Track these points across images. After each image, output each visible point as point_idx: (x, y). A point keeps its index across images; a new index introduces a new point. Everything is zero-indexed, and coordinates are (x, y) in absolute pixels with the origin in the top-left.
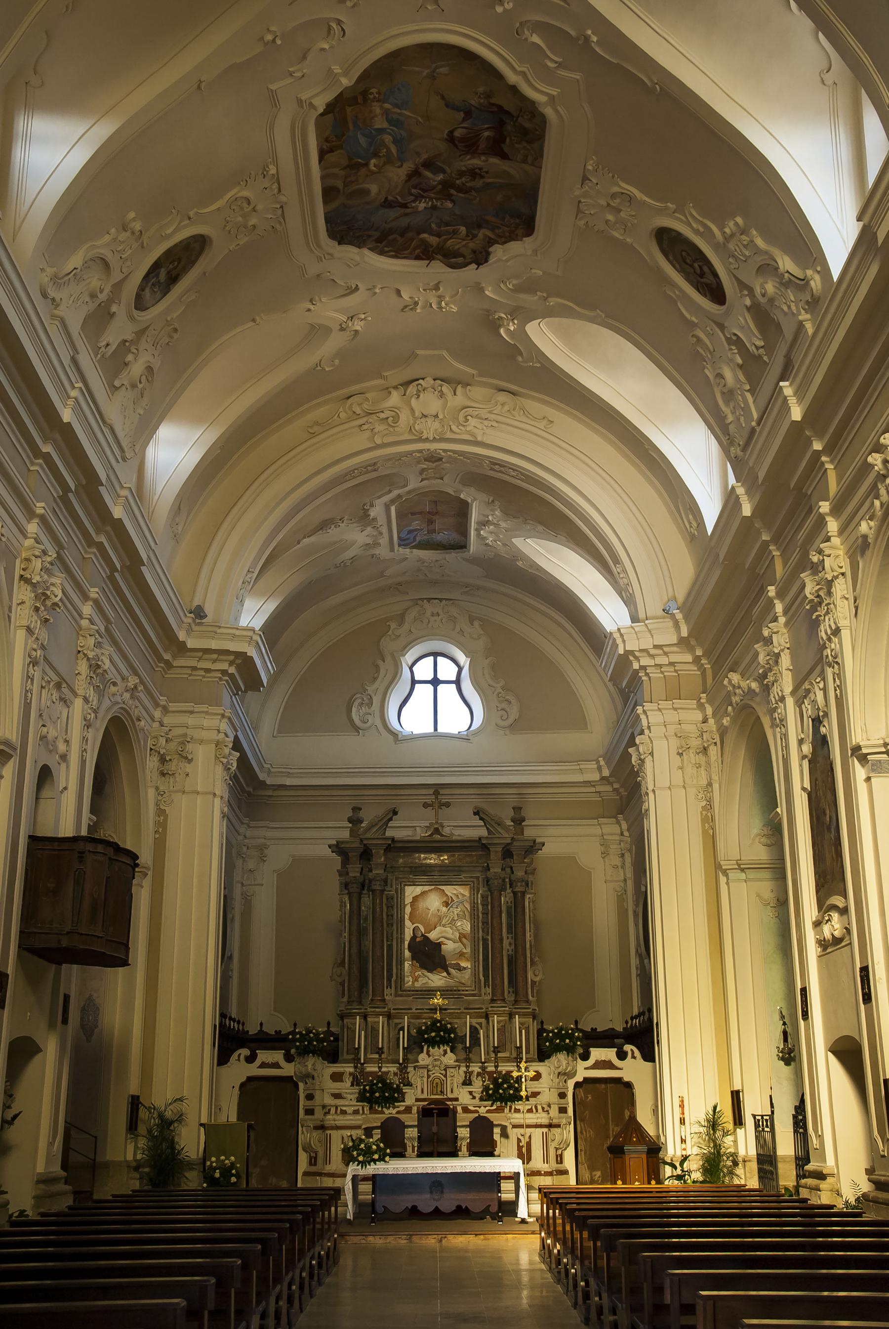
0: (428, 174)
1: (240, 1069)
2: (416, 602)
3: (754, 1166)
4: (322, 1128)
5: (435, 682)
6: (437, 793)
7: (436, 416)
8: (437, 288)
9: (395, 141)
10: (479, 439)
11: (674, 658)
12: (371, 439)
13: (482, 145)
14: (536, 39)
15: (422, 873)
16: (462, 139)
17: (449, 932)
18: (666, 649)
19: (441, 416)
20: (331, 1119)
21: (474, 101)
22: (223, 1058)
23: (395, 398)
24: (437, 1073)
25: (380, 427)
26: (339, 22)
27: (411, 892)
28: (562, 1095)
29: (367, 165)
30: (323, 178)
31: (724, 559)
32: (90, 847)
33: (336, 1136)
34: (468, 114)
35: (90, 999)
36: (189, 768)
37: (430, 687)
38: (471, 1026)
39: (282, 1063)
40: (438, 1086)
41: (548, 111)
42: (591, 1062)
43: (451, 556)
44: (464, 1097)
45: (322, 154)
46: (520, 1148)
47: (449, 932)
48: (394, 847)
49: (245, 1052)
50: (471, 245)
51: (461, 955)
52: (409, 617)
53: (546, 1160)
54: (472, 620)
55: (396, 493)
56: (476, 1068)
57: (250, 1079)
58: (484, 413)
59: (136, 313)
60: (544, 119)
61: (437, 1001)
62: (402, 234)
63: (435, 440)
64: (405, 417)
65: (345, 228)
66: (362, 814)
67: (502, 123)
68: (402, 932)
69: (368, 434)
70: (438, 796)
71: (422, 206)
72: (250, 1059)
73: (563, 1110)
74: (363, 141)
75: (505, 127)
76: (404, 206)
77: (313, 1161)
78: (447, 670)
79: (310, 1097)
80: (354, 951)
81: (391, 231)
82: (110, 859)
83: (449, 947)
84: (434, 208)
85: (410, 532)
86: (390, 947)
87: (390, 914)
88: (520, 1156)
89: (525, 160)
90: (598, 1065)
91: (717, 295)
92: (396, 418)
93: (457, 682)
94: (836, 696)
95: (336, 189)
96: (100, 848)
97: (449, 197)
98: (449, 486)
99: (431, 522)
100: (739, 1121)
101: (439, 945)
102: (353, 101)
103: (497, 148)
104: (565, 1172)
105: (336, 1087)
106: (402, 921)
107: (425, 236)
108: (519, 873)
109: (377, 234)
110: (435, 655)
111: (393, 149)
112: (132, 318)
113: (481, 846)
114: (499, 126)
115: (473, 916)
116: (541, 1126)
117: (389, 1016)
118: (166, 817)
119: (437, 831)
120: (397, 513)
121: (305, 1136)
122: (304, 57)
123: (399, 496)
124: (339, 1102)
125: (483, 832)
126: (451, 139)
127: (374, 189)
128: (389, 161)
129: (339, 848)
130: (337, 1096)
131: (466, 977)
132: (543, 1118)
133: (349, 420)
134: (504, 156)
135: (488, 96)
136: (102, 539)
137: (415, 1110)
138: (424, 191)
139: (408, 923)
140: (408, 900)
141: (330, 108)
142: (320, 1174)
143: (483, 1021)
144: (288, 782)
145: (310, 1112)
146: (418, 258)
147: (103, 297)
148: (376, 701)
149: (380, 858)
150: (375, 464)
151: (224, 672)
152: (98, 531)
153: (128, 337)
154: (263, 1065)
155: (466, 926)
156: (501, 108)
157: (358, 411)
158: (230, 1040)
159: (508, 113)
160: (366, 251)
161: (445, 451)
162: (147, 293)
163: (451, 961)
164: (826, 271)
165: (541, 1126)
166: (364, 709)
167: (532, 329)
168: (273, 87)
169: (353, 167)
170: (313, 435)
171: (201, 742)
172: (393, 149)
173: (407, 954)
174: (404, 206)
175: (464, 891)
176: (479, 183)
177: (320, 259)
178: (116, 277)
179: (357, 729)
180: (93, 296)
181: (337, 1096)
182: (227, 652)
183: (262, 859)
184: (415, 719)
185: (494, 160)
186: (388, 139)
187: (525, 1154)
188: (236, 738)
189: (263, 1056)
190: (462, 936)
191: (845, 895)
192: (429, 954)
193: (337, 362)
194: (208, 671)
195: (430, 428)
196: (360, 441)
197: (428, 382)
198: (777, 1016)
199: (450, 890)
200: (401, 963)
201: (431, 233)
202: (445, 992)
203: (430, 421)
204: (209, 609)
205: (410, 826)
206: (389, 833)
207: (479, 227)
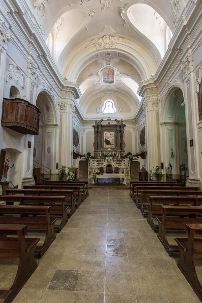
3: (165, 175)
4: (91, 168)
5: (109, 106)
7: (109, 43)
10: (116, 48)
11: (152, 86)
15: (106, 130)
17: (111, 139)
18: (151, 84)
19: (109, 43)
23: (101, 40)
27: (105, 133)
31: (172, 49)
33: (93, 170)
35: (49, 147)
36: (65, 108)
37: (108, 107)
38: (114, 153)
40: (109, 162)
43: (111, 84)
44: (113, 164)
47: (111, 139)
48: (102, 126)
49: (80, 157)
51: (113, 142)
52: (105, 96)
54: (114, 96)
55: (102, 68)
56: (115, 159)
61: (109, 149)
64: (103, 43)
68: (104, 139)
69: (96, 48)
72: (80, 158)
73: (129, 166)
77: (90, 173)
78: (111, 104)
80: (96, 142)
82: (26, 105)
83: (111, 141)
85: (105, 79)
86: (102, 141)
87: (102, 135)
92: (101, 43)
93: (112, 106)
94: (187, 88)
96: (23, 102)
99: (108, 76)
100: (162, 168)
101: (109, 141)
104: (129, 175)
105: (93, 162)
106: (103, 137)
108: (122, 130)
110: (109, 102)
113: (116, 125)
115: (115, 137)
116: (125, 168)
117: (102, 152)
118: (62, 117)
119: (109, 123)
120: (103, 73)
121: (89, 169)
124: (94, 164)
130: (93, 163)
131: (114, 146)
132: (126, 167)
137: (105, 166)
143: (116, 152)
144: (88, 120)
145: (89, 166)
148: (100, 108)
149: (100, 127)
150: (98, 55)
151: (71, 92)
152: (60, 87)
154: (82, 159)
155: (114, 138)
157: (94, 43)
158: (75, 155)
161: (110, 51)
163: (111, 143)
165: (125, 168)
166: (99, 110)
171: (68, 104)
173: (104, 142)
175: (113, 133)
179: (97, 113)
181: (93, 163)
182: (71, 87)
183: (84, 131)
184: (106, 111)
189: (82, 158)
192: (108, 142)
193: (89, 28)
194: (68, 91)
196: (94, 49)
197: (107, 36)
199: (111, 132)
200: (103, 144)
202: (110, 148)
203: (107, 44)
206: (101, 123)
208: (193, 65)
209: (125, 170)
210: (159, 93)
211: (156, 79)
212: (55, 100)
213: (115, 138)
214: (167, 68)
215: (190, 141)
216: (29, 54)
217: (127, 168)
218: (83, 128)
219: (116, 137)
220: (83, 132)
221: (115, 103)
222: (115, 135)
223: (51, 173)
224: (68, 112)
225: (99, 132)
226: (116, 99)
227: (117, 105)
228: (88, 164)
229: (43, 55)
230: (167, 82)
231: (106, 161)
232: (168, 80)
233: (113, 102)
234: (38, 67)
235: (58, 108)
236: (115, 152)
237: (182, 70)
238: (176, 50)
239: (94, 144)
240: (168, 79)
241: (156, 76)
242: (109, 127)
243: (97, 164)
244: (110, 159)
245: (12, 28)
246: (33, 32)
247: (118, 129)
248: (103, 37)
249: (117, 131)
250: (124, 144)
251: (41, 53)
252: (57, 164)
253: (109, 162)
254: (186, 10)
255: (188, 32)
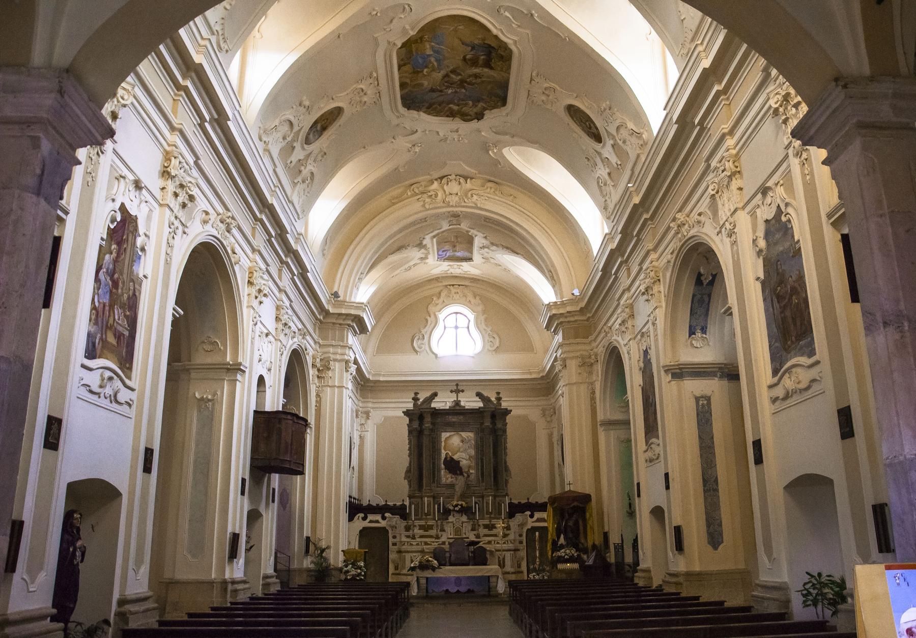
0: (453, 76)
1: (359, 523)
2: (446, 286)
4: (399, 552)
5: (456, 327)
6: (457, 385)
8: (457, 131)
9: (436, 61)
12: (424, 206)
13: (481, 62)
14: (507, 14)
16: (470, 60)
20: (404, 548)
21: (476, 42)
22: (351, 519)
23: (436, 185)
24: (457, 525)
25: (428, 200)
26: (409, 5)
27: (444, 435)
28: (521, 535)
29: (422, 71)
30: (400, 78)
32: (284, 416)
33: (408, 557)
34: (473, 48)
39: (380, 520)
41: (513, 48)
42: (535, 518)
45: (400, 67)
46: (499, 561)
47: (464, 455)
48: (436, 413)
49: (362, 515)
50: (475, 110)
51: (470, 467)
52: (443, 294)
53: (512, 566)
57: (364, 528)
58: (481, 193)
59: (306, 146)
60: (511, 51)
62: (440, 105)
63: (456, 206)
64: (440, 194)
65: (411, 101)
66: (419, 396)
67: (490, 53)
68: (440, 453)
70: (457, 387)
71: (450, 91)
72: (364, 519)
74: (420, 61)
75: (492, 54)
76: (441, 91)
77: (396, 568)
79: (394, 537)
81: (434, 104)
83: (464, 463)
84: (456, 92)
88: (500, 565)
89: (502, 70)
90: (539, 520)
91: (598, 138)
92: (436, 195)
93: (468, 328)
95: (406, 83)
97: (464, 87)
98: (464, 226)
101: (459, 462)
102: (416, 42)
103: (488, 64)
104: (522, 572)
107: (451, 106)
108: (499, 425)
109: (427, 105)
111: (435, 64)
112: (303, 149)
114: (489, 54)
116: (509, 550)
121: (393, 556)
122: (391, 21)
123: (438, 234)
125: (481, 405)
126: (464, 59)
127: (426, 83)
128: (434, 70)
129: (407, 413)
132: (511, 546)
133: (412, 196)
134: (491, 68)
135: (484, 40)
136: (188, 83)
138: (451, 84)
139: (443, 451)
140: (443, 439)
141: (404, 45)
142: (399, 574)
144: (382, 379)
145: (394, 544)
146: (448, 116)
147: (289, 139)
148: (426, 337)
152: (184, 77)
153: (302, 158)
154: (371, 522)
155: (472, 452)
156: (489, 46)
159: (493, 48)
160: (422, 113)
162: (311, 136)
164: (650, 130)
165: (509, 550)
166: (420, 342)
167: (505, 151)
168: (375, 36)
169: (416, 72)
170: (394, 204)
172: (435, 64)
173: (443, 466)
174: (441, 91)
175: (471, 435)
176: (479, 80)
177: (398, 117)
178: (296, 128)
180: (284, 138)
185: (486, 70)
186: (433, 59)
187: (502, 564)
188: (355, 358)
189: (371, 517)
190: (470, 457)
191: (658, 438)
192: (453, 466)
195: (454, 200)
197: (453, 177)
198: (626, 496)
199: (464, 434)
200: (439, 471)
201: (455, 104)
204: (341, 293)
205: (443, 402)
206: (433, 405)
207: (479, 101)
208: (740, 189)
209: (508, 555)
210: (655, 249)
211: (636, 200)
212: (236, 268)
213: (477, 453)
214: (598, 297)
215: (754, 442)
216: (172, 128)
217: (516, 550)
218: (365, 405)
219: (480, 448)
220: (363, 422)
221: (476, 319)
222: (476, 442)
223: (292, 567)
224: (336, 384)
225: (426, 432)
226: (480, 308)
227: (484, 327)
228: (391, 540)
229: (216, 120)
230: (674, 219)
231: (449, 529)
232: (680, 211)
233: (471, 316)
234: (196, 163)
235: (312, 372)
236: (479, 497)
237: (713, 195)
238: (689, 121)
239: (408, 471)
240: (678, 206)
241: (637, 191)
242: (457, 416)
243: (408, 537)
244: (463, 522)
245: (294, 305)
246: (198, 58)
247: (487, 423)
248: (442, 178)
249: (482, 431)
250: (507, 469)
251: (276, 231)
252: (308, 538)
253: (457, 531)
254: (643, 160)
255: (645, 216)
